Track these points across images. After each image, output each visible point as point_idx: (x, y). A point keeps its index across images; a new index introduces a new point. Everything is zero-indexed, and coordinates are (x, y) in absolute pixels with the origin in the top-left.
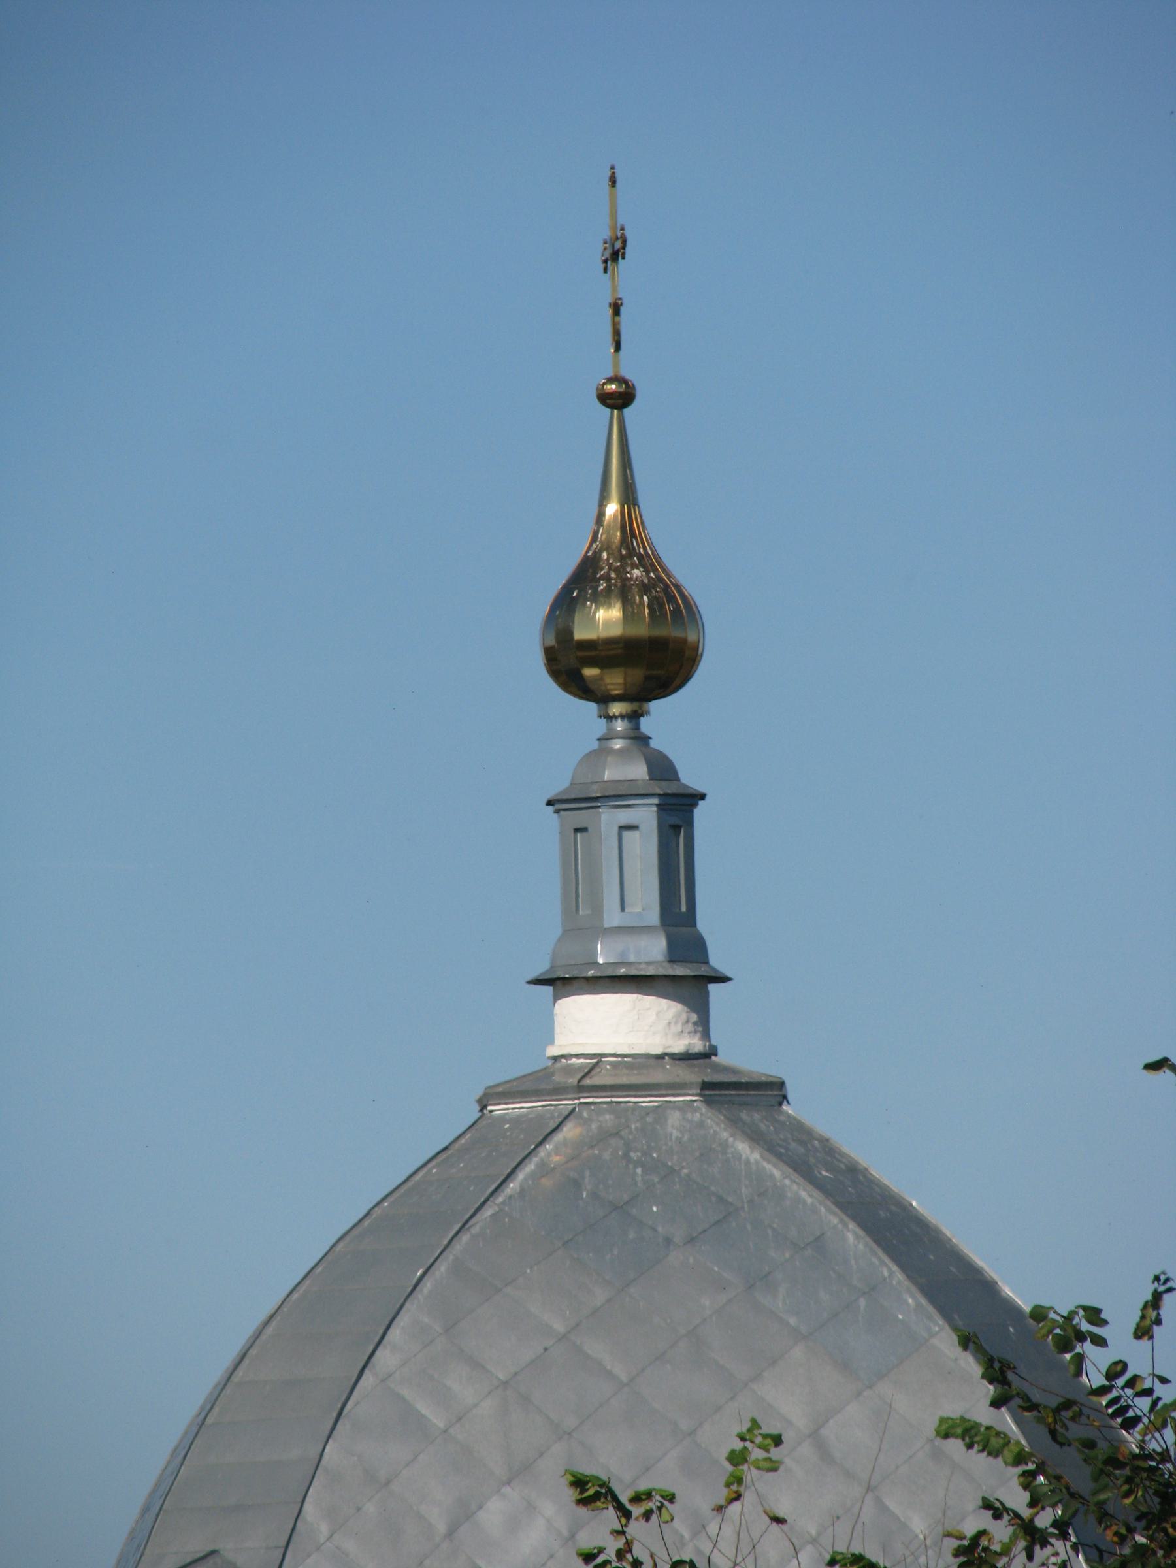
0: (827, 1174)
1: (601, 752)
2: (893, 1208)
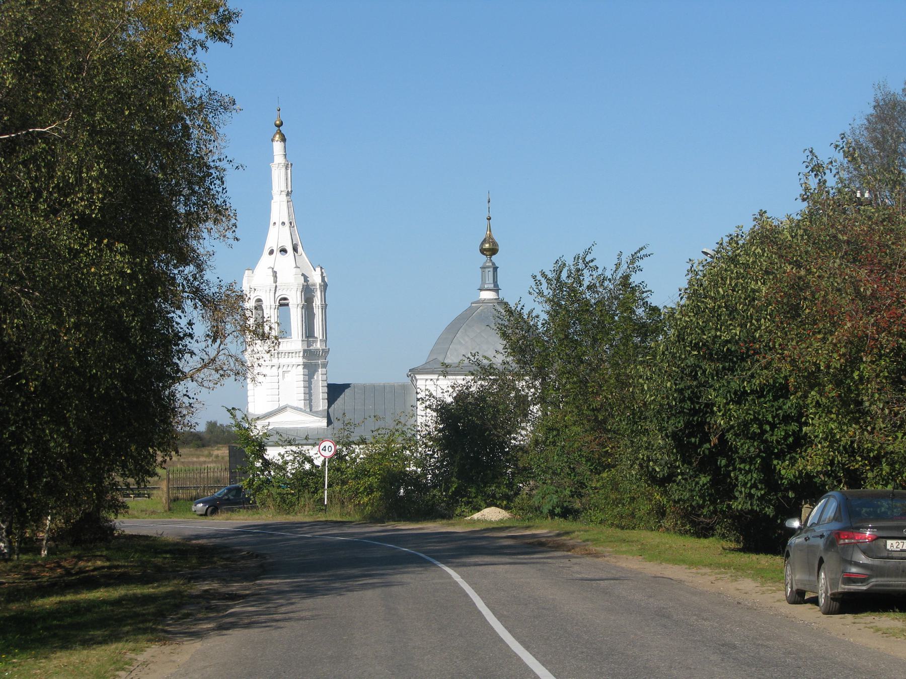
0: (279, 209)
2: (112, 581)
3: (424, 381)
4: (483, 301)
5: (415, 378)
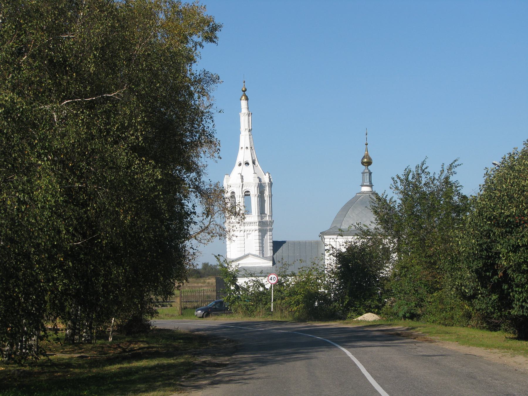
0: (245, 139)
1: (365, 170)
3: (329, 239)
4: (363, 193)
5: (324, 237)
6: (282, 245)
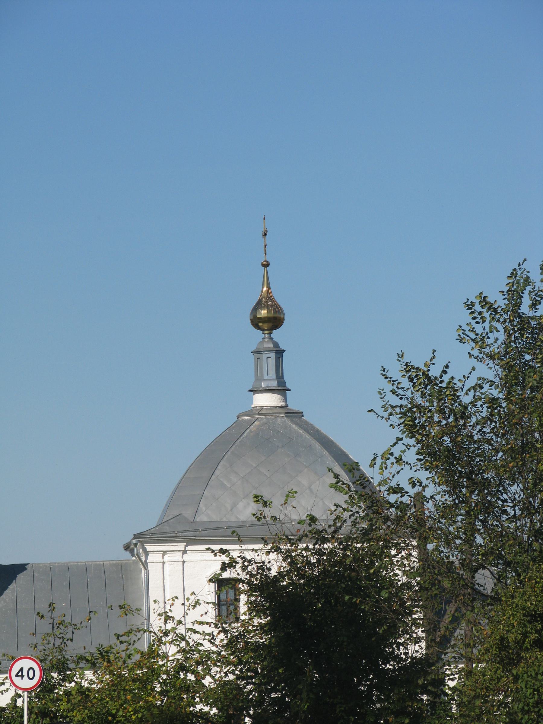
1: (263, 341)
3: (160, 555)
4: (261, 411)
5: (144, 549)
6: (15, 577)
